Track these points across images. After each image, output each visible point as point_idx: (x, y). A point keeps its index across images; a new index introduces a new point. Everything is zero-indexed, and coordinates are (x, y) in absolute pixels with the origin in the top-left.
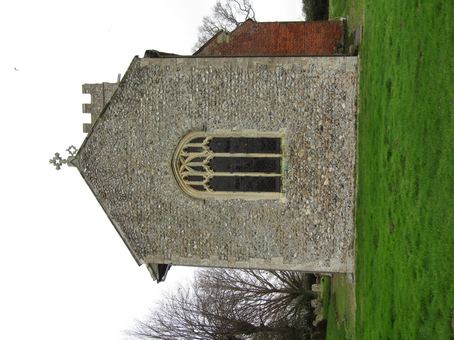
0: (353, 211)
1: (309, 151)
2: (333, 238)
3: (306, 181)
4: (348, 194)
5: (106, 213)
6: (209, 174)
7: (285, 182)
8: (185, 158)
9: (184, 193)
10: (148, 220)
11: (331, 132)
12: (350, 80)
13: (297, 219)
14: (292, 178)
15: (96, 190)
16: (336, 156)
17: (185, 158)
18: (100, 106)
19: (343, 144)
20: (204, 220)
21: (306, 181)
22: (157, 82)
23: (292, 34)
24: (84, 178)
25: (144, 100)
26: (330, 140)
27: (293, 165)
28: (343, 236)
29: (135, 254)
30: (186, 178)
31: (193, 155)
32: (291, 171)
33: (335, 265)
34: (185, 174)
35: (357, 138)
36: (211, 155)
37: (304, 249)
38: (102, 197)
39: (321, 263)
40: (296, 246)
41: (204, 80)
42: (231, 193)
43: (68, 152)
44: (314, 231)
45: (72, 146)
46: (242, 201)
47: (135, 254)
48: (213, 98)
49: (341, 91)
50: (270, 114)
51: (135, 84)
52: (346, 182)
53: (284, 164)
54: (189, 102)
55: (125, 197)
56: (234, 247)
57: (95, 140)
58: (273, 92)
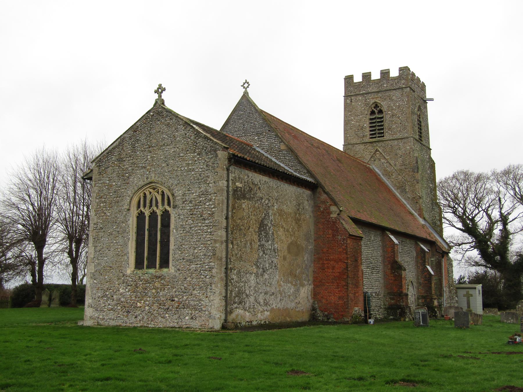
0: (120, 325)
1: (159, 291)
2: (105, 310)
3: (140, 289)
4: (131, 321)
5: (124, 133)
6: (147, 213)
7: (139, 272)
8: (158, 192)
9: (134, 194)
10: (119, 166)
11: (170, 308)
12: (203, 323)
13: (117, 282)
14: (142, 278)
15: (139, 123)
16: (155, 311)
17: (158, 192)
18: (387, 86)
19: (162, 317)
20: (117, 211)
21: (140, 289)
22: (207, 166)
23: (338, 274)
24: (147, 113)
25: (195, 156)
26: (165, 307)
27: (151, 278)
28: (106, 318)
29: (99, 159)
30: (145, 194)
31: (159, 198)
32: (146, 277)
33: (89, 311)
34: (147, 193)
35: (141, 328)
36: (159, 213)
37: (99, 288)
38: (134, 129)
39: (90, 301)
40: (101, 281)
41: (207, 204)
42: (135, 230)
43: (244, 82)
44: (109, 296)
45: (249, 85)
46: (129, 239)
47: (99, 159)
48: (195, 212)
49: (197, 315)
50: (183, 259)
51: (206, 147)
52: (138, 319)
53: (152, 271)
54: (193, 193)
55: (134, 148)
56: (101, 234)
57: (171, 119)
58: (198, 261)
